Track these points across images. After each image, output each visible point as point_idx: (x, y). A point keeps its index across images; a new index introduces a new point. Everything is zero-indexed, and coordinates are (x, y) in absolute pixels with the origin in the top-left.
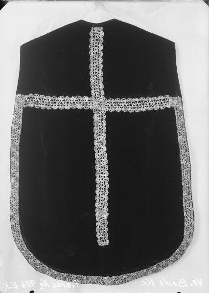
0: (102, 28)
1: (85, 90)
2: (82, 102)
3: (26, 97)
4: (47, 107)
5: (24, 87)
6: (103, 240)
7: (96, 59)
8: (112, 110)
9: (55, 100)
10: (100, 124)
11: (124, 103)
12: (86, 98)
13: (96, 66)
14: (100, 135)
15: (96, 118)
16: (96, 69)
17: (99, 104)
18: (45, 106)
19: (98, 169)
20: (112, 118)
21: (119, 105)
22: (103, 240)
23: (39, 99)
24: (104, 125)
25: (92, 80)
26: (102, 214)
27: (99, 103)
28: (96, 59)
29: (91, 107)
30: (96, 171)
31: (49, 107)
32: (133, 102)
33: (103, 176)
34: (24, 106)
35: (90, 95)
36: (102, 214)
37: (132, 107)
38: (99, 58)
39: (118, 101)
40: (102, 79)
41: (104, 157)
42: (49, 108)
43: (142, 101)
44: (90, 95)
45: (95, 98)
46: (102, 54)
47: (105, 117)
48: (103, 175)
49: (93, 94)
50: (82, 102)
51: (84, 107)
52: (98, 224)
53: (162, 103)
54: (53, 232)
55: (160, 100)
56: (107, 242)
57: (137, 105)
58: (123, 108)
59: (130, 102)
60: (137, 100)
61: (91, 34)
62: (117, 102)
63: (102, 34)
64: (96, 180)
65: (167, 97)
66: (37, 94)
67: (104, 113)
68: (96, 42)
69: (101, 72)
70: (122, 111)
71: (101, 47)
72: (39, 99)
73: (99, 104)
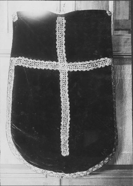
0: (64, 18)
1: (53, 57)
2: (52, 65)
3: (17, 58)
4: (29, 66)
5: (15, 53)
6: (65, 151)
7: (60, 38)
8: (71, 70)
9: (34, 62)
10: (64, 79)
11: (79, 65)
12: (55, 62)
13: (61, 42)
14: (64, 87)
15: (61, 76)
16: (64, 85)
17: (63, 67)
18: (28, 66)
19: (63, 109)
20: (72, 76)
21: (76, 67)
22: (65, 151)
23: (25, 60)
24: (67, 80)
25: (58, 51)
26: (65, 137)
27: (63, 65)
28: (60, 38)
29: (58, 69)
30: (61, 109)
31: (31, 66)
32: (85, 64)
33: (64, 72)
34: (16, 65)
35: (57, 61)
36: (65, 137)
37: (84, 67)
38: (67, 102)
39: (75, 64)
40: (64, 51)
41: (67, 100)
42: (30, 67)
43: (91, 63)
44: (57, 61)
45: (61, 62)
46: (64, 34)
47: (67, 75)
48: (66, 112)
49: (59, 60)
50: (52, 65)
51: (54, 68)
52: (62, 143)
53: (103, 63)
54: (34, 137)
55: (102, 61)
56: (68, 154)
57: (88, 66)
58: (79, 69)
59: (83, 64)
60: (88, 62)
61: (57, 21)
62: (75, 65)
63: (64, 21)
64: (62, 115)
65: (106, 58)
66: (23, 57)
67: (66, 72)
68: (65, 116)
69: (64, 46)
70: (78, 71)
71: (64, 30)
72: (25, 60)
73: (63, 67)
